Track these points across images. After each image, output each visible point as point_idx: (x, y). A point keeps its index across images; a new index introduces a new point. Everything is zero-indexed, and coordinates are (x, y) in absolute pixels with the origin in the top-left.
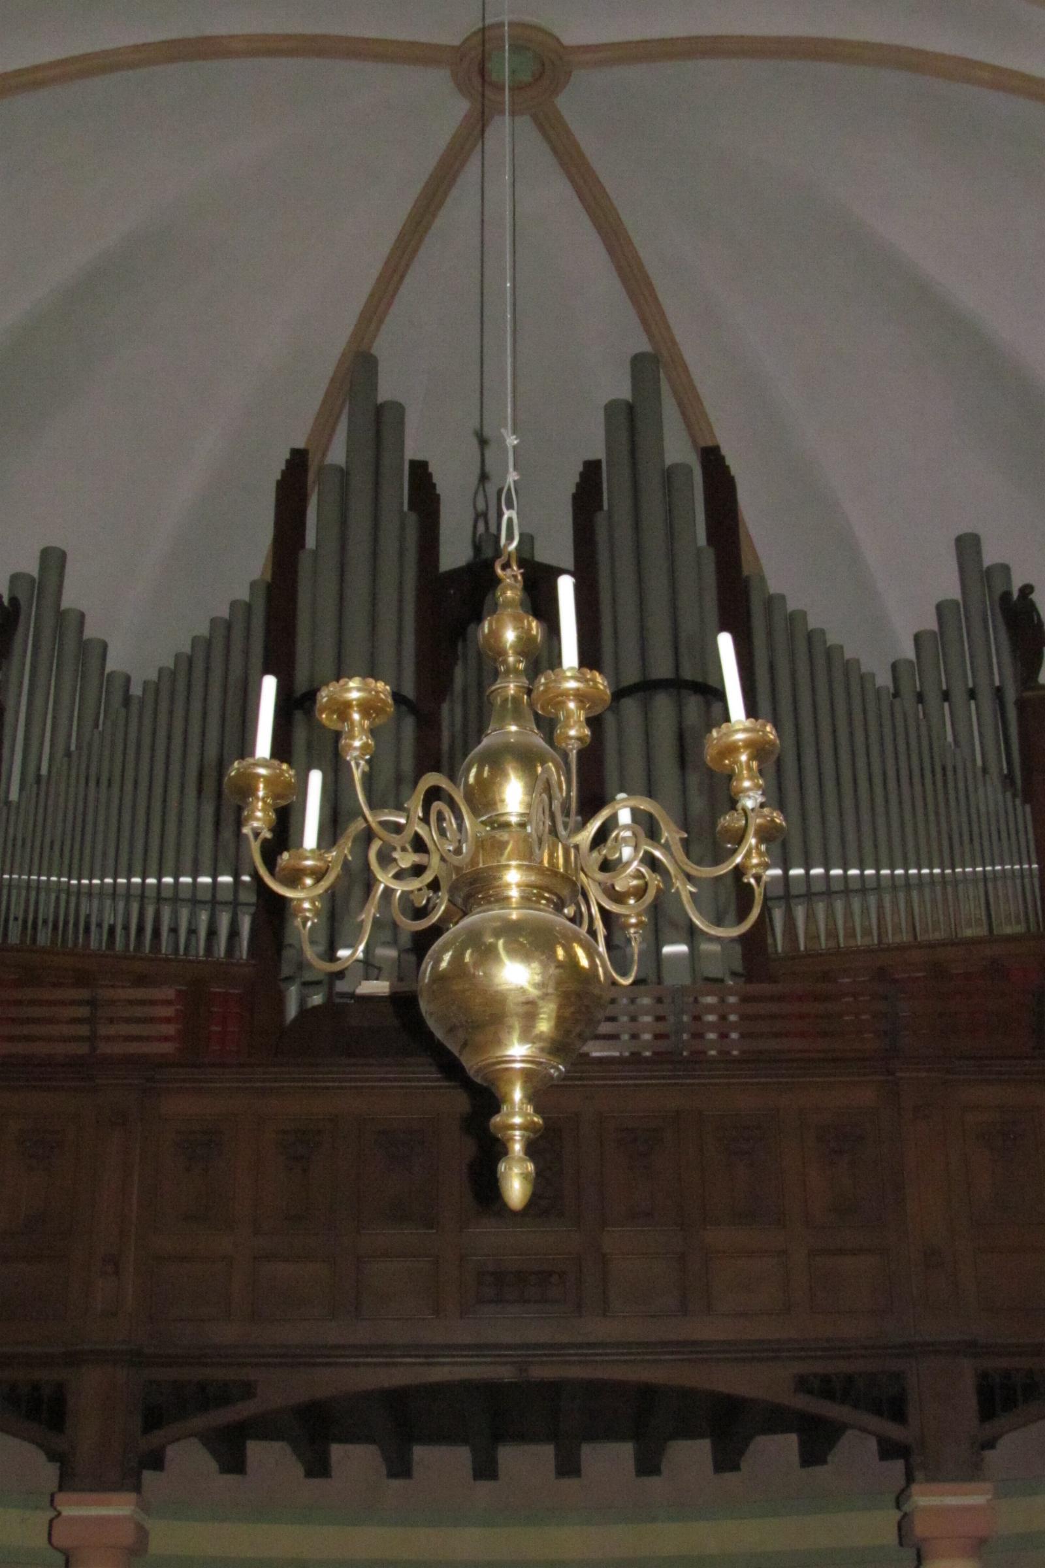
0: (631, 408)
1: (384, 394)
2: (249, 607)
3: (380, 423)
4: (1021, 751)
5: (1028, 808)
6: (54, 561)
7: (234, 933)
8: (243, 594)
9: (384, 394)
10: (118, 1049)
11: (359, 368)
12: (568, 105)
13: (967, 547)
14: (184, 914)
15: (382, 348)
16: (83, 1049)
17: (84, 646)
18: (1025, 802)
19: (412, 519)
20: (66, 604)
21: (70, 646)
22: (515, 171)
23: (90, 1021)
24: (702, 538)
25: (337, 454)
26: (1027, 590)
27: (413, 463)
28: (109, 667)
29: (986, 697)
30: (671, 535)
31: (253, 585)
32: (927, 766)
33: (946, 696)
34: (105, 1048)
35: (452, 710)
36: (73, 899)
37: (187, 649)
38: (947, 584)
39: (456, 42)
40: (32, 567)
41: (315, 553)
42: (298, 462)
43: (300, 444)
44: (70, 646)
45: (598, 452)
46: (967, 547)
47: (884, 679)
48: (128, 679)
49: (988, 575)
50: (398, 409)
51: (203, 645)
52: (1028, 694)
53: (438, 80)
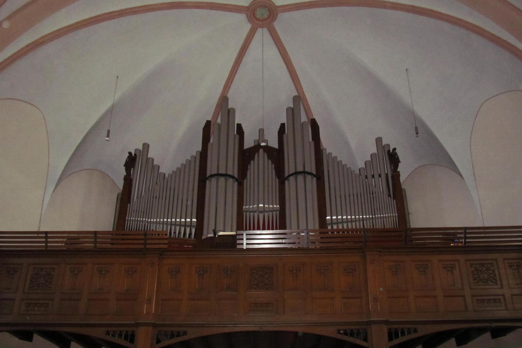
0: (293, 109)
1: (230, 106)
2: (195, 158)
3: (230, 113)
4: (393, 191)
5: (395, 201)
6: (146, 146)
7: (190, 234)
8: (194, 154)
9: (230, 106)
10: (152, 246)
11: (224, 100)
12: (277, 25)
13: (379, 140)
14: (178, 228)
15: (230, 95)
16: (142, 246)
17: (153, 166)
18: (394, 199)
19: (237, 136)
20: (149, 156)
21: (150, 166)
22: (262, 35)
23: (145, 239)
24: (311, 140)
25: (219, 121)
26: (394, 149)
27: (237, 124)
28: (160, 171)
29: (383, 176)
30: (303, 137)
31: (197, 152)
32: (368, 192)
33: (373, 176)
34: (148, 246)
35: (247, 182)
36: (149, 224)
37: (180, 167)
38: (374, 150)
39: (246, 5)
40: (140, 147)
41: (212, 144)
42: (208, 124)
43: (209, 119)
44: (150, 166)
45: (284, 121)
46: (379, 140)
47: (357, 172)
48: (165, 174)
49: (384, 147)
50: (234, 110)
51: (184, 166)
52: (395, 174)
53: (241, 18)
